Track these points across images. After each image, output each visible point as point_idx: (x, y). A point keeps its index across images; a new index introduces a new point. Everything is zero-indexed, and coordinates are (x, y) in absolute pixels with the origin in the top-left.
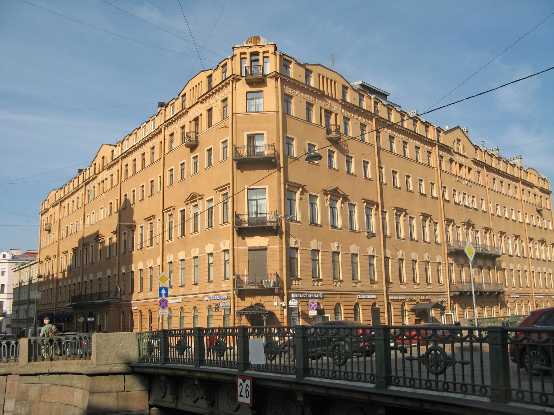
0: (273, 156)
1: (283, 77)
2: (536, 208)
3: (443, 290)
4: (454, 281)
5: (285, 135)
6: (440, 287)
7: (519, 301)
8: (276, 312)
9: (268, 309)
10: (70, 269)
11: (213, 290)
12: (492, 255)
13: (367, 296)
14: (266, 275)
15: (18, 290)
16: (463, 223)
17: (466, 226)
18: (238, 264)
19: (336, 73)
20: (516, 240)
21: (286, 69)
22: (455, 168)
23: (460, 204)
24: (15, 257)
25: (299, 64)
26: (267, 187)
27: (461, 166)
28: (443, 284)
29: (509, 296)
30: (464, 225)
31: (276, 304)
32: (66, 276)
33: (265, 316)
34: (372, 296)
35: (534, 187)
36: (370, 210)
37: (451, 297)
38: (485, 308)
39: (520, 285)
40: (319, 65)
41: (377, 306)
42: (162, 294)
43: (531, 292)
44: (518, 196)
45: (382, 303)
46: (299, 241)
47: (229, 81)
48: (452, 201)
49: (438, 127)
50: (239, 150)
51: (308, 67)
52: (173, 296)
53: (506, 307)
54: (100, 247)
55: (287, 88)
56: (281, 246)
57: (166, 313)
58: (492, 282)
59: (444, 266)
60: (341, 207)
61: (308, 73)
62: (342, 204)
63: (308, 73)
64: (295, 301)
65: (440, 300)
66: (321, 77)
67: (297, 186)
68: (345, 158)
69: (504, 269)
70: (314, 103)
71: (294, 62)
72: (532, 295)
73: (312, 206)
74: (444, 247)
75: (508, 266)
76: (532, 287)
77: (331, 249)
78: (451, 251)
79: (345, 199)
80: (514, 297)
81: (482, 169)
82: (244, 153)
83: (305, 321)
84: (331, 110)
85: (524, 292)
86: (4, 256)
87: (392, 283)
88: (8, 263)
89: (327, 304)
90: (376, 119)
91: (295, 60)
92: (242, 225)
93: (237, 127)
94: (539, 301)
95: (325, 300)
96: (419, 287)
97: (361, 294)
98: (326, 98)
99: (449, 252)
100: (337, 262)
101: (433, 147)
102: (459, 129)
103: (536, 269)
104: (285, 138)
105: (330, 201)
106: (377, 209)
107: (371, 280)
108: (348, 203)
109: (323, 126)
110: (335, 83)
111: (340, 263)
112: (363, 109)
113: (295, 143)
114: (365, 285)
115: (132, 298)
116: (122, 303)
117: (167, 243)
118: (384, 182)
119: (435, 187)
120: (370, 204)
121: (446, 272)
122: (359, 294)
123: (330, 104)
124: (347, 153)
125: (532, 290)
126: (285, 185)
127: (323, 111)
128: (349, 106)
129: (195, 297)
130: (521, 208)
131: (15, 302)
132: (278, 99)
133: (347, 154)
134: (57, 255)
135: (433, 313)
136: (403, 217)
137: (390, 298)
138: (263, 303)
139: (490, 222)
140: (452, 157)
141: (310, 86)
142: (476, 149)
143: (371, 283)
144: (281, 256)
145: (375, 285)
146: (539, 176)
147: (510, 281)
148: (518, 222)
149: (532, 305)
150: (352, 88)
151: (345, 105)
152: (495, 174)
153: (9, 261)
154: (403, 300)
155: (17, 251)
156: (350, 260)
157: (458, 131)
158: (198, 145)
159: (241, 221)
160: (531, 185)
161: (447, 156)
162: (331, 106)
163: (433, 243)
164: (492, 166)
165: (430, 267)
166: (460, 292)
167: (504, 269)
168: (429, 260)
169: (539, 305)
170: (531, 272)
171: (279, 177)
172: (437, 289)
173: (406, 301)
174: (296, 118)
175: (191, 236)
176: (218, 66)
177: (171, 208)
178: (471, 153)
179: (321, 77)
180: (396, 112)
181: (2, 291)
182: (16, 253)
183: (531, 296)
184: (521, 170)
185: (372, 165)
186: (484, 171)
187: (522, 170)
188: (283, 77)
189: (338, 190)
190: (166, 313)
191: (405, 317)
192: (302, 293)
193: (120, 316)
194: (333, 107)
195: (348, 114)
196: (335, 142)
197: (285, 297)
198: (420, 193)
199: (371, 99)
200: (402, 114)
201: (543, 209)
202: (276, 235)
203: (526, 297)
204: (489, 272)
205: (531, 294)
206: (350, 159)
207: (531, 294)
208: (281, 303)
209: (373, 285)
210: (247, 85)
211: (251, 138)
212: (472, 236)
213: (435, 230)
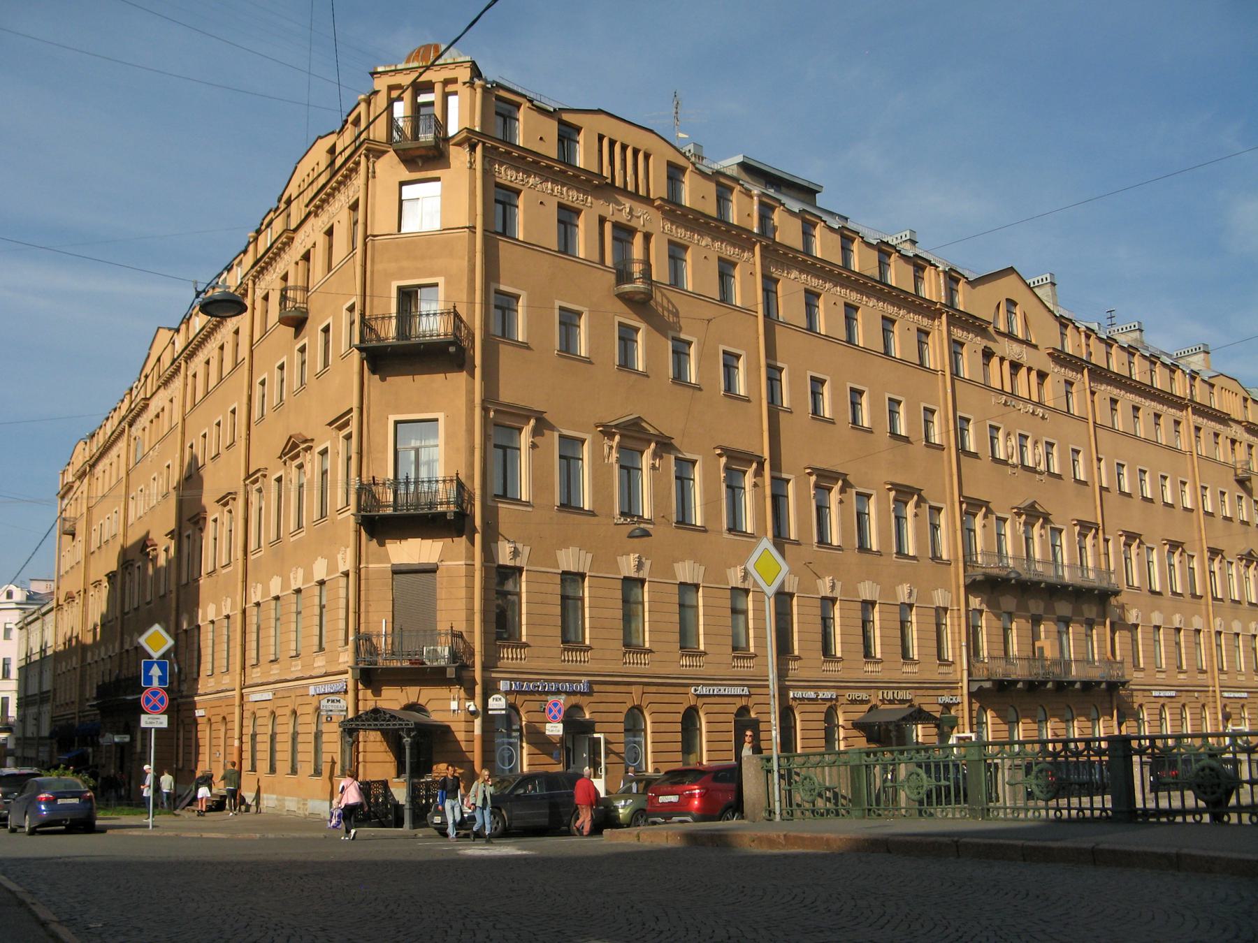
0: (451, 338)
1: (489, 143)
2: (1236, 475)
3: (951, 678)
4: (986, 655)
5: (493, 286)
6: (944, 669)
7: (1174, 705)
8: (454, 727)
9: (436, 717)
10: (106, 622)
11: (323, 671)
12: (1095, 589)
13: (722, 688)
14: (431, 635)
15: (26, 671)
16: (1015, 510)
17: (1024, 517)
18: (367, 606)
19: (651, 131)
20: (1213, 560)
21: (505, 122)
22: (997, 374)
23: (1010, 461)
24: (35, 597)
25: (542, 111)
26: (440, 416)
27: (1015, 366)
28: (953, 662)
29: (1147, 693)
30: (1019, 514)
31: (454, 705)
32: (98, 638)
33: (409, 736)
34: (738, 691)
35: (1230, 423)
36: (742, 475)
37: (970, 695)
38: (1075, 723)
39: (1180, 667)
40: (600, 111)
41: (753, 715)
42: (151, 677)
43: (1210, 682)
44: (1183, 444)
45: (764, 709)
46: (526, 551)
47: (360, 156)
48: (1179, 507)
49: (951, 269)
50: (377, 325)
51: (566, 117)
52: (262, 684)
53: (1137, 719)
54: (150, 571)
55: (503, 169)
56: (472, 563)
57: (161, 723)
58: (1096, 657)
59: (956, 615)
60: (653, 467)
61: (568, 134)
62: (654, 459)
63: (568, 134)
64: (339, 701)
65: (940, 701)
66: (606, 143)
67: (524, 414)
68: (670, 344)
69: (1136, 626)
70: (581, 207)
71: (528, 104)
72: (1214, 691)
73: (898, 521)
74: (957, 568)
75: (1147, 618)
76: (1213, 672)
77: (618, 570)
78: (975, 580)
79: (664, 445)
80: (1162, 695)
81: (1079, 376)
82: (389, 331)
83: (539, 749)
84: (633, 223)
85: (1189, 683)
86: (10, 595)
87: (798, 658)
88: (18, 611)
89: (602, 707)
90: (763, 249)
91: (531, 101)
92: (379, 511)
93: (375, 269)
94: (1234, 705)
95: (596, 697)
96: (879, 667)
97: (704, 685)
98: (619, 195)
99: (969, 581)
100: (637, 603)
101: (934, 320)
102: (1013, 277)
103: (1228, 626)
104: (492, 294)
105: (894, 503)
106: (759, 472)
107: (735, 649)
108: (673, 457)
109: (607, 264)
110: (647, 157)
111: (646, 605)
112: (813, 256)
113: (583, 322)
114: (718, 660)
115: (198, 689)
116: (180, 700)
117: (253, 557)
118: (785, 405)
119: (1081, 457)
120: (737, 460)
121: (960, 633)
122: (698, 685)
123: (628, 210)
124: (676, 331)
125: (1213, 678)
126: (485, 410)
127: (608, 227)
128: (696, 220)
129: (295, 688)
130: (1190, 473)
131: (43, 698)
132: (476, 196)
133: (675, 335)
134: (82, 590)
135: (920, 733)
136: (913, 506)
137: (791, 696)
138: (424, 704)
139: (1096, 508)
140: (991, 344)
141: (680, 206)
142: (1064, 326)
143: (734, 657)
144: (470, 587)
145: (747, 663)
146: (1247, 396)
147: (1153, 656)
148: (1237, 522)
149: (1213, 716)
150: (697, 169)
151: (672, 208)
152: (1117, 387)
153: (20, 606)
154: (831, 699)
155: (44, 584)
156: (676, 599)
157: (1012, 278)
158: (307, 319)
159: (378, 501)
160: (1223, 418)
161: (973, 344)
162: (632, 216)
163: (1188, 597)
164: (1174, 393)
165: (914, 619)
166: (995, 682)
167: (1136, 626)
168: (913, 600)
169: (1233, 716)
170: (1213, 633)
171: (471, 392)
172: (934, 673)
173: (838, 704)
174: (970, 381)
175: (292, 539)
176: (346, 121)
177: (259, 474)
178: (1047, 335)
179: (606, 143)
180: (786, 214)
181: (6, 675)
182: (40, 588)
183: (1211, 694)
184: (1193, 378)
185: (748, 363)
186: (1083, 380)
187: (1198, 380)
188: (489, 143)
189: (644, 424)
190: (161, 723)
191: (837, 742)
192: (530, 681)
193: (178, 731)
194: (639, 217)
195: (681, 234)
196: (640, 304)
197: (478, 689)
198: (1143, 496)
199: (751, 197)
200: (847, 238)
201: (1253, 477)
202: (460, 535)
203: (1196, 694)
204: (1089, 633)
205: (1211, 688)
206: (735, 361)
207: (1211, 688)
208: (467, 704)
209: (741, 663)
210: (402, 166)
211: (408, 296)
212: (1043, 543)
213: (935, 527)
